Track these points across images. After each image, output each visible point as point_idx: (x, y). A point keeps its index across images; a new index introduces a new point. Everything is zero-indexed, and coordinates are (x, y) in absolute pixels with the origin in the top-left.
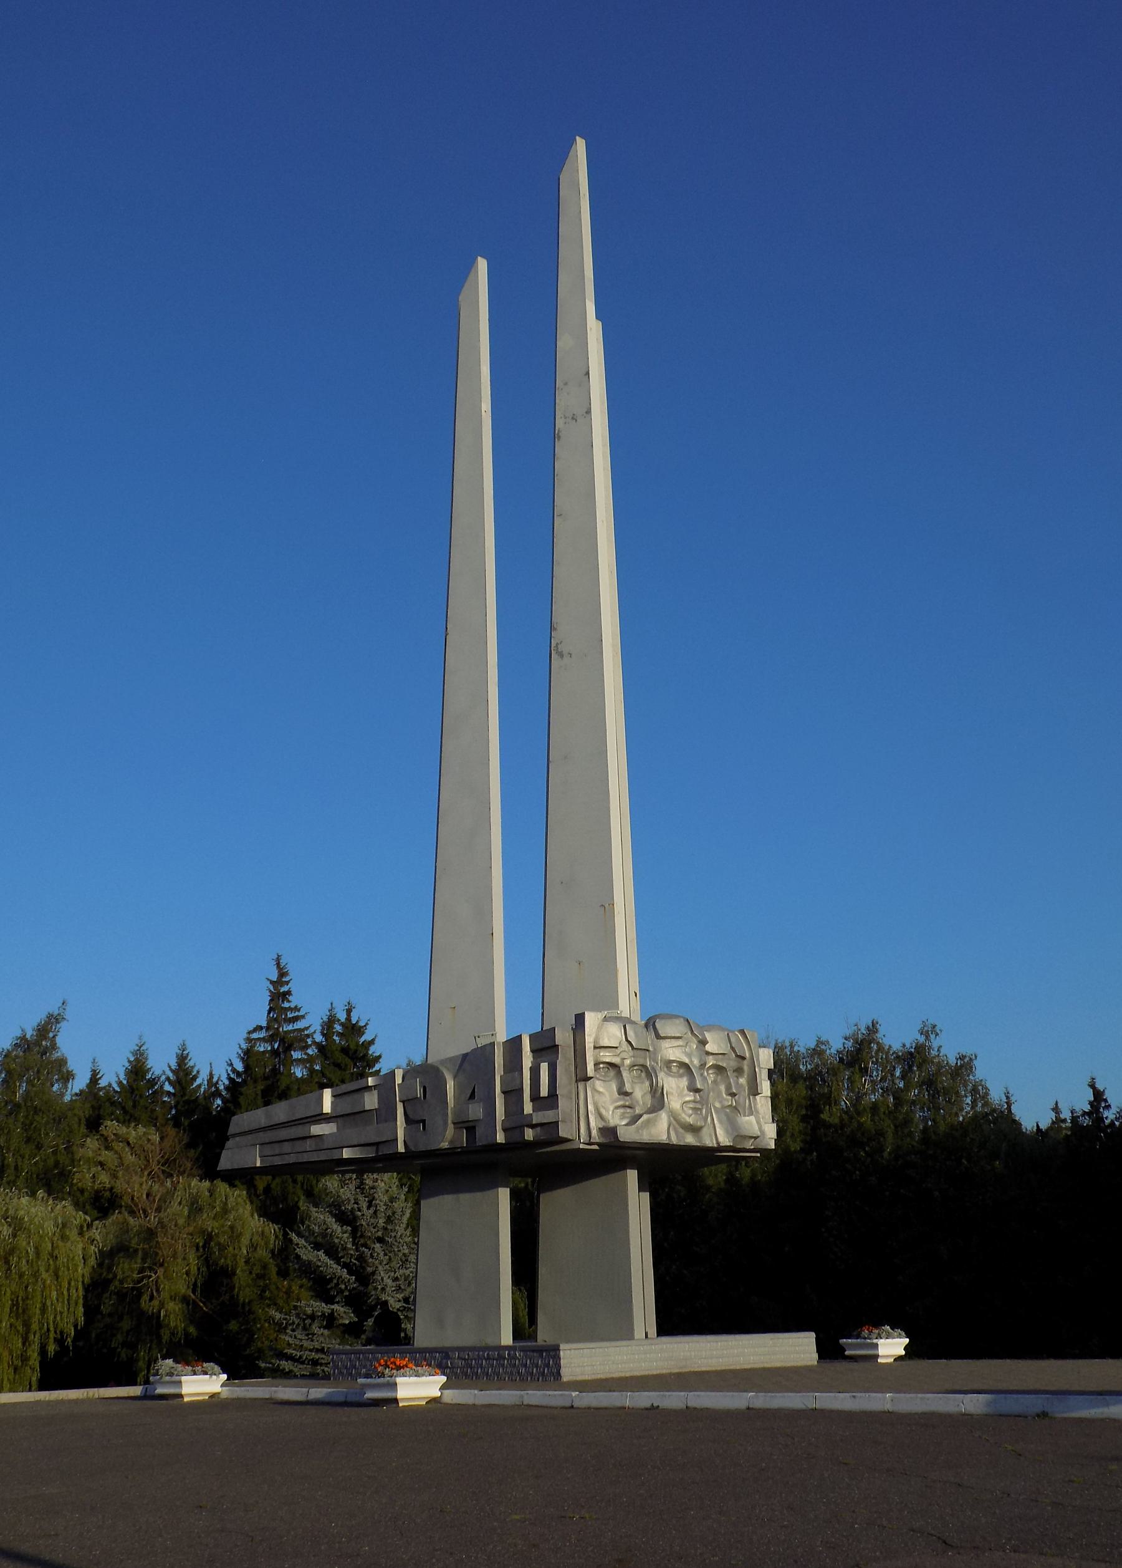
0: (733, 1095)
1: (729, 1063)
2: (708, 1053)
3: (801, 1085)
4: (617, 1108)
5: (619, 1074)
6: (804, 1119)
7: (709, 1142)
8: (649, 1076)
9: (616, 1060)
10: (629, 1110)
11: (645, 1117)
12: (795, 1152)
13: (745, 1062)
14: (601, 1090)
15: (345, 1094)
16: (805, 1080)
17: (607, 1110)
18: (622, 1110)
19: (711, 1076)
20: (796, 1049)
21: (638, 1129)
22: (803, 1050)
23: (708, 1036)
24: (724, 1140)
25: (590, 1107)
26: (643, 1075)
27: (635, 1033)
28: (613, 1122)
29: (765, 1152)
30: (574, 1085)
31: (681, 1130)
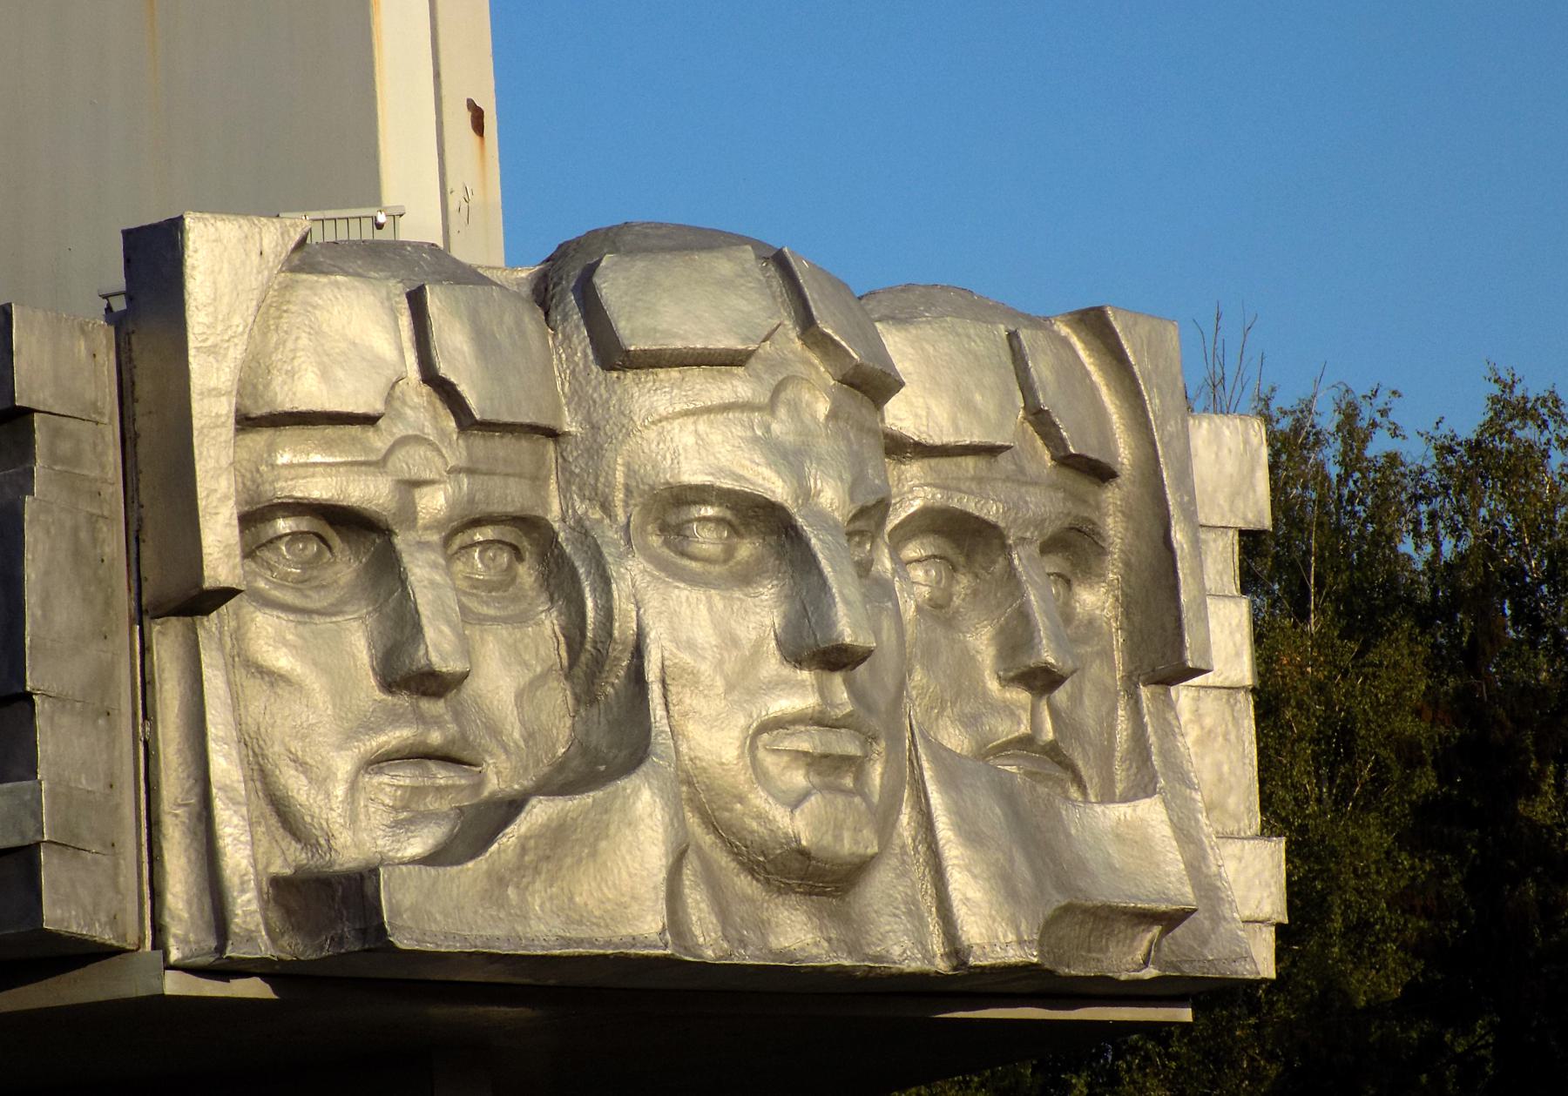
0: (1042, 681)
1: (1023, 501)
2: (899, 447)
3: (1402, 657)
4: (378, 762)
5: (386, 570)
6: (1425, 828)
7: (902, 944)
8: (559, 579)
10: (443, 776)
11: (539, 812)
12: (1376, 1009)
13: (1112, 496)
14: (282, 661)
16: (1425, 616)
17: (320, 781)
18: (405, 777)
19: (917, 578)
20: (1379, 446)
21: (498, 881)
22: (1417, 453)
23: (900, 348)
24: (991, 931)
25: (224, 765)
26: (527, 574)
27: (482, 338)
28: (350, 847)
29: (1220, 996)
30: (123, 639)
31: (745, 884)
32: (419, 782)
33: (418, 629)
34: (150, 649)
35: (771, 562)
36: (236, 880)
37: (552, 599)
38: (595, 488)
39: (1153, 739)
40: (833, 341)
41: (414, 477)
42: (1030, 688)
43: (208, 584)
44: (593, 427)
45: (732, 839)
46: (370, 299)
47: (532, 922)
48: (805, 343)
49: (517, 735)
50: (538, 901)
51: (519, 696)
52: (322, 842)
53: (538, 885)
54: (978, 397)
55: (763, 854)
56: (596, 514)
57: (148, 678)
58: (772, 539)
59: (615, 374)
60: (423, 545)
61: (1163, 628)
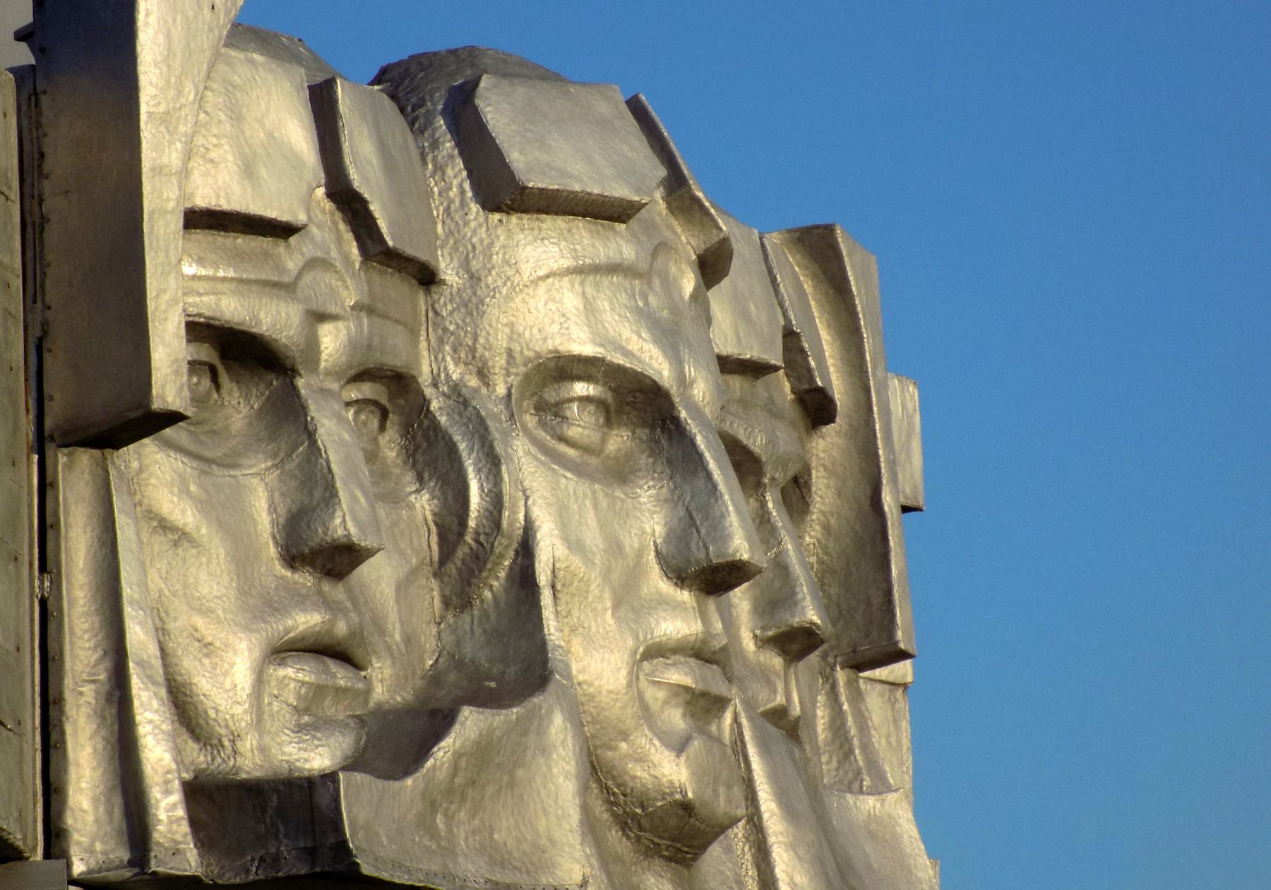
5: (287, 415)
9: (273, 319)
10: (341, 675)
11: (471, 723)
15: (828, 841)
32: (324, 680)
33: (331, 493)
34: (54, 485)
35: (644, 460)
36: (158, 779)
37: (420, 479)
38: (473, 350)
39: (853, 732)
40: (702, 206)
41: (322, 309)
42: (784, 652)
43: (156, 405)
44: (472, 277)
45: (610, 783)
46: (287, 85)
47: (460, 859)
48: (669, 207)
49: (398, 637)
50: (463, 835)
51: (399, 589)
52: (226, 743)
53: (463, 815)
54: (752, 307)
55: (643, 807)
56: (473, 382)
57: (49, 521)
58: (644, 433)
59: (497, 216)
60: (325, 392)
61: (869, 604)
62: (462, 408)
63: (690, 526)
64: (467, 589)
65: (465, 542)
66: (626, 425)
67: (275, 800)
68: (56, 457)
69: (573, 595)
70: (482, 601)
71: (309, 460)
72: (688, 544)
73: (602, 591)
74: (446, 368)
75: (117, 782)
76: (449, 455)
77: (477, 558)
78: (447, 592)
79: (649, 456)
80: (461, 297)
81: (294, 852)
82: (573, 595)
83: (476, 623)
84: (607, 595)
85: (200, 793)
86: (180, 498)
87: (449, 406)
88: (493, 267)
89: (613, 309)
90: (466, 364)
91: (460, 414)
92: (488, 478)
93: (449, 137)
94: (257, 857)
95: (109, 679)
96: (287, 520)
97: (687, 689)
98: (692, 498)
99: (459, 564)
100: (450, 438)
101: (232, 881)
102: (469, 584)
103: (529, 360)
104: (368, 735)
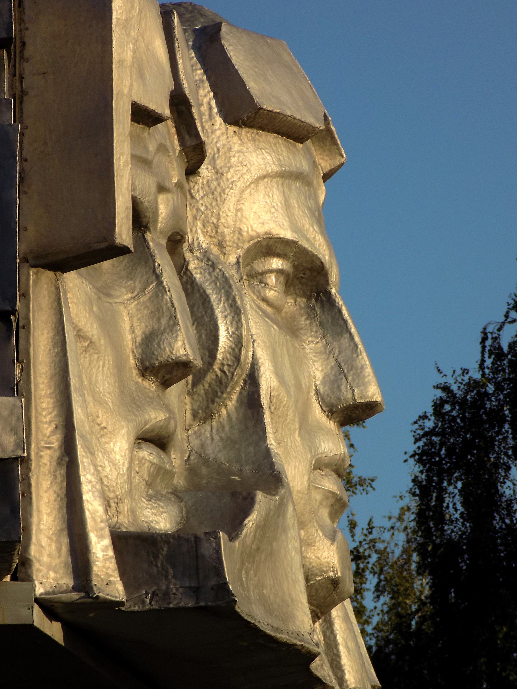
38: (216, 227)
44: (217, 172)
58: (302, 301)
62: (211, 270)
63: (340, 374)
64: (211, 405)
65: (213, 370)
66: (292, 294)
67: (165, 549)
68: (29, 274)
69: (279, 417)
70: (220, 415)
71: (157, 296)
72: (339, 387)
73: (294, 416)
74: (198, 239)
75: (65, 525)
76: (203, 304)
77: (221, 383)
78: (196, 407)
79: (307, 319)
80: (209, 186)
81: (181, 590)
82: (279, 417)
83: (214, 431)
84: (297, 419)
85: (121, 541)
86: (90, 315)
87: (201, 268)
88: (231, 167)
89: (299, 207)
90: (210, 236)
91: (210, 274)
92: (232, 323)
93: (199, 66)
94: (150, 592)
95: (60, 447)
96: (142, 340)
97: (333, 494)
98: (340, 352)
99: (207, 386)
100: (204, 292)
101: (132, 609)
102: (213, 402)
103: (252, 238)
104: (186, 506)
